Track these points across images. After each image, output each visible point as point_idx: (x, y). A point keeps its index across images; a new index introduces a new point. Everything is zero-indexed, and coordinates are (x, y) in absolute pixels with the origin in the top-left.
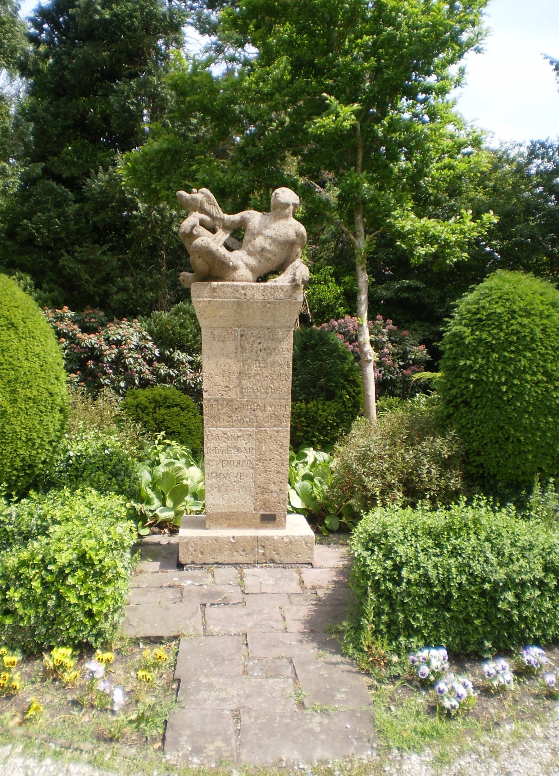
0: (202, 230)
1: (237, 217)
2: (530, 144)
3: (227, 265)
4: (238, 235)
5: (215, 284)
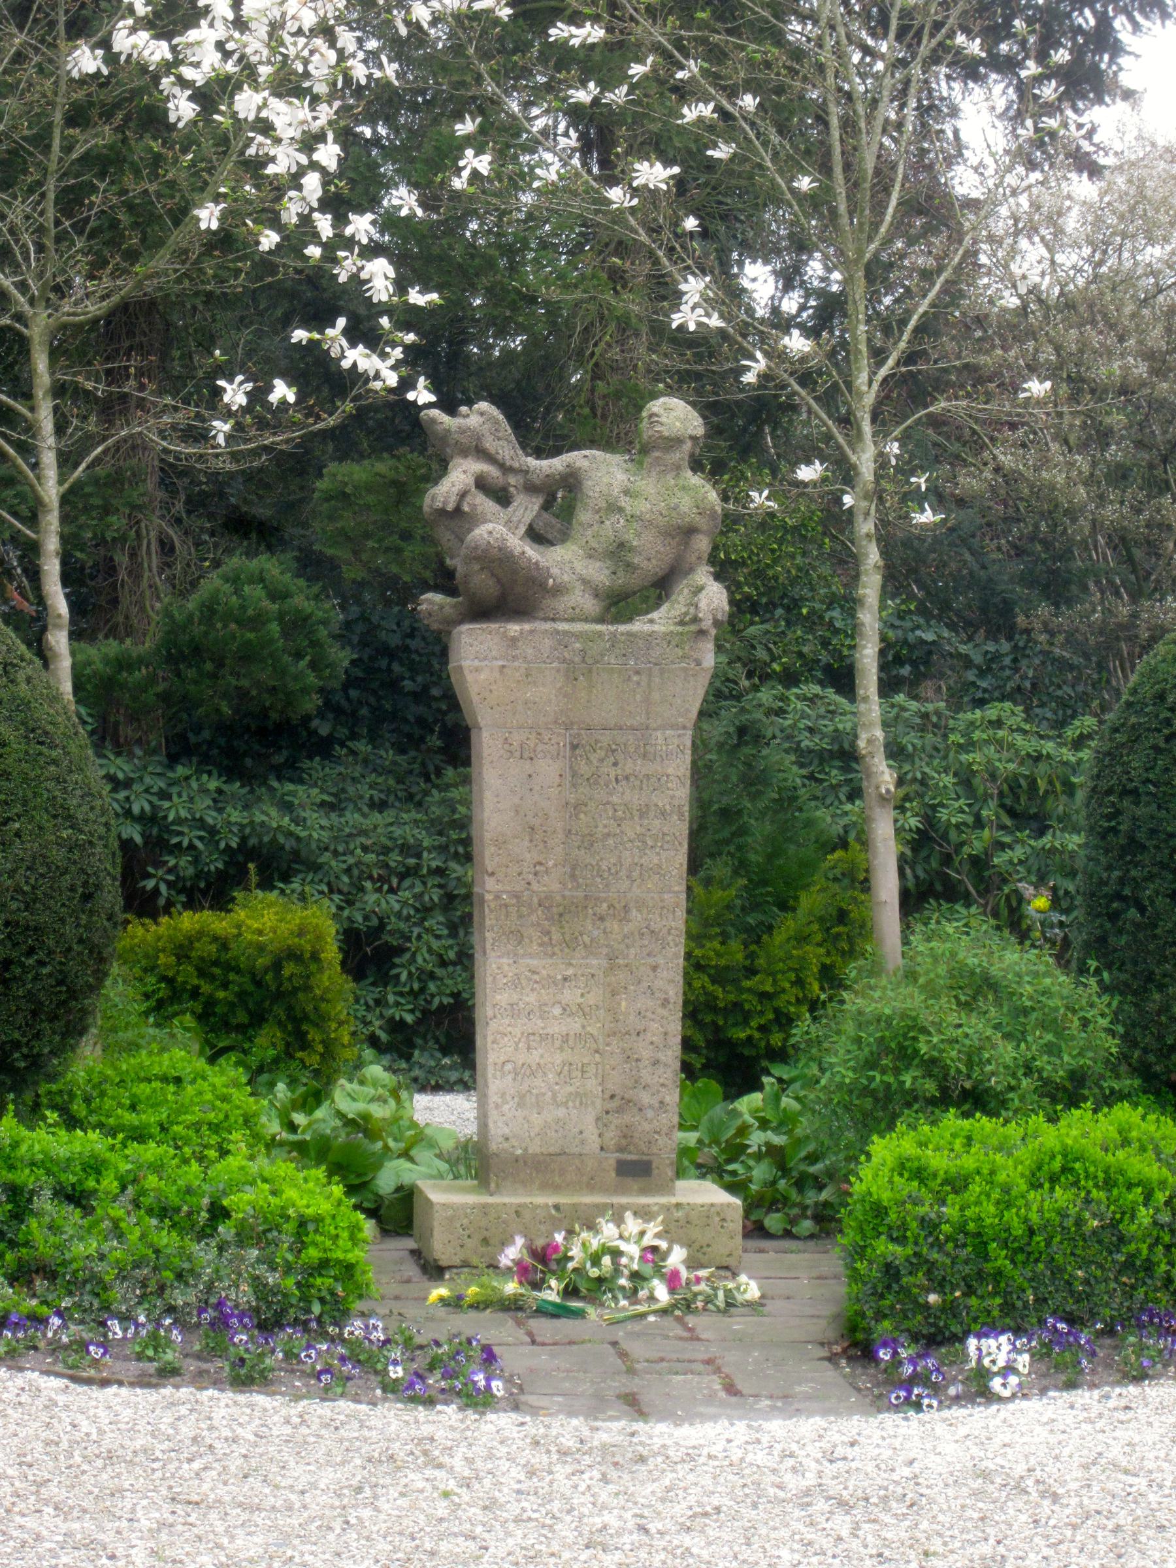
0: (485, 504)
1: (556, 464)
3: (543, 586)
4: (560, 502)
5: (514, 628)
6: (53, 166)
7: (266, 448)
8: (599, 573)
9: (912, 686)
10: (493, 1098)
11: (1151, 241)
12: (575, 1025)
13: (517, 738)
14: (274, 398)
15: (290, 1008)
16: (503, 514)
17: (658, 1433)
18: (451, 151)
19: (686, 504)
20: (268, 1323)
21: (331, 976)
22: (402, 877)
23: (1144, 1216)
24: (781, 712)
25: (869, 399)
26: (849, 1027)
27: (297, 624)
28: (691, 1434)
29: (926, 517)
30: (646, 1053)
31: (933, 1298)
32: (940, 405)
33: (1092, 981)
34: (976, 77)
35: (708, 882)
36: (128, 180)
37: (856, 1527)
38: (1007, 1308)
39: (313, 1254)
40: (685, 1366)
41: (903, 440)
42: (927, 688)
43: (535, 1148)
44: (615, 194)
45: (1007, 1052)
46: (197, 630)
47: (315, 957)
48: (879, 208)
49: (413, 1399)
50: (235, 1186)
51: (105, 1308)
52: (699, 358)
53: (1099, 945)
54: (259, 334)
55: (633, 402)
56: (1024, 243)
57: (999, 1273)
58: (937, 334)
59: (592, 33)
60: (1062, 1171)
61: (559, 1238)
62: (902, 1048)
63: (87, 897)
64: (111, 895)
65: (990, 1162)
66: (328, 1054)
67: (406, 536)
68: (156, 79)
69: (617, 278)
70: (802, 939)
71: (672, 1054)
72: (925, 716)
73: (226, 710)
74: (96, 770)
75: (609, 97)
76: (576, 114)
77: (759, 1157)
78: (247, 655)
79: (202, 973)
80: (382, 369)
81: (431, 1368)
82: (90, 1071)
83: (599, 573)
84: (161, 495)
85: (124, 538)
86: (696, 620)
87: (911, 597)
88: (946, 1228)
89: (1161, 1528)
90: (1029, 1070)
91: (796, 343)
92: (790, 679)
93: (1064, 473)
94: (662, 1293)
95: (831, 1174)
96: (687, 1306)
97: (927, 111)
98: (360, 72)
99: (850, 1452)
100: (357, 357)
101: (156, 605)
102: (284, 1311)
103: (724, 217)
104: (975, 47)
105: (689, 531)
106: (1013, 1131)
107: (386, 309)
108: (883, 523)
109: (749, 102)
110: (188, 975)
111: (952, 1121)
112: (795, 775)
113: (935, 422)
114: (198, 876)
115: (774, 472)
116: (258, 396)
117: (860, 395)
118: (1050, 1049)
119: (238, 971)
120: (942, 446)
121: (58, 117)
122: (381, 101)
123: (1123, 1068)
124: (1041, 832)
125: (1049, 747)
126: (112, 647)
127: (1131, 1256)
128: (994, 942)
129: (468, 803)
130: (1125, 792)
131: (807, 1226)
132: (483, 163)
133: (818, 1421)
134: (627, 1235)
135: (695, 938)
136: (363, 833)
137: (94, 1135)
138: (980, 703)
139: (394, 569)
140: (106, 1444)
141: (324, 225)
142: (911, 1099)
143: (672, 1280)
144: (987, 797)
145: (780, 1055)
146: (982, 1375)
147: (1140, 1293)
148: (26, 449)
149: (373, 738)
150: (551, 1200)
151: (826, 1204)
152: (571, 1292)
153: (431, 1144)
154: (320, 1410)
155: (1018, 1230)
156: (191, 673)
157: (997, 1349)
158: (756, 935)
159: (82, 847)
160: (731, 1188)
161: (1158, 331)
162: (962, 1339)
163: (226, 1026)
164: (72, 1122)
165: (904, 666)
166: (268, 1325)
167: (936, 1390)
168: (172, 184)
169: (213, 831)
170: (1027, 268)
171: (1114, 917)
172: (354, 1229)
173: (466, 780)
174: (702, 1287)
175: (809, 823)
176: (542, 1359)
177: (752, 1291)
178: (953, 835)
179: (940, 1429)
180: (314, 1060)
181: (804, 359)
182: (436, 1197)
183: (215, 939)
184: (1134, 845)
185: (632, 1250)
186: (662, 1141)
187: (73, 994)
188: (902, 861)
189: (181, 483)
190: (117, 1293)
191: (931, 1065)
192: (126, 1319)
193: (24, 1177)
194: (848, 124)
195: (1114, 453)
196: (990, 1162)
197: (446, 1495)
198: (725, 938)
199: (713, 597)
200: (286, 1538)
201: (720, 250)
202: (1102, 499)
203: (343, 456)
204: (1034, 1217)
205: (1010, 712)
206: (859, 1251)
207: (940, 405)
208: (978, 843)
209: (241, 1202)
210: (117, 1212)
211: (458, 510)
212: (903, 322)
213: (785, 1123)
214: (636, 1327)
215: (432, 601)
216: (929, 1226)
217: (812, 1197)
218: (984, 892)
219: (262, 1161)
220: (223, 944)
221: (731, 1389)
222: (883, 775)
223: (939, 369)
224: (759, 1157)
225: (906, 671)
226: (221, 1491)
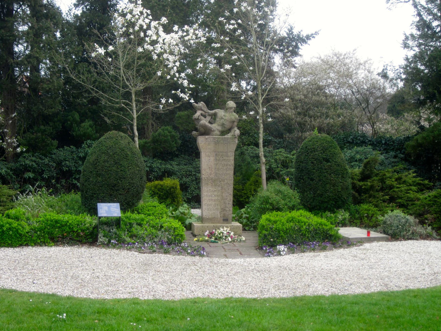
1: (213, 111)
2: (337, 52)
3: (211, 130)
5: (207, 137)
6: (135, 66)
7: (168, 109)
8: (220, 128)
9: (267, 146)
10: (204, 209)
11: (304, 78)
12: (216, 198)
13: (207, 154)
14: (169, 102)
15: (172, 196)
16: (205, 119)
17: (230, 260)
18: (196, 64)
19: (233, 117)
20: (169, 243)
21: (178, 190)
22: (189, 176)
23: (304, 227)
24: (247, 150)
25: (261, 102)
26: (258, 198)
27: (173, 137)
28: (235, 261)
29: (270, 120)
30: (227, 202)
31: (272, 240)
32: (272, 103)
33: (296, 191)
34: (277, 53)
35: (236, 176)
36: (147, 68)
37: (261, 275)
38: (283, 241)
39: (176, 233)
40: (233, 250)
41: (266, 108)
42: (270, 146)
43: (210, 217)
44: (222, 70)
45: (283, 202)
46: (157, 138)
47: (176, 188)
48: (263, 73)
49: (192, 255)
50: (164, 223)
51: (144, 241)
52: (235, 95)
53: (297, 185)
54: (166, 92)
55: (225, 103)
56: (284, 78)
57: (282, 236)
58: (271, 92)
59: (218, 45)
60: (292, 220)
61: (214, 231)
62: (267, 201)
63: (141, 178)
64: (145, 178)
65: (281, 219)
66: (178, 203)
67: (190, 123)
68: (151, 52)
69: (222, 83)
70: (251, 185)
71: (231, 202)
72: (269, 151)
73: (162, 150)
74: (143, 159)
75: (221, 55)
76: (215, 58)
77: (244, 218)
78: (165, 142)
79: (158, 190)
80: (186, 97)
81: (195, 251)
82: (141, 205)
83: (220, 128)
84: (152, 117)
85: (146, 124)
86: (235, 135)
87: (267, 132)
88: (274, 229)
89: (308, 275)
90: (286, 205)
91: (250, 93)
92: (249, 145)
93: (291, 113)
94: (230, 239)
95: (256, 221)
96: (234, 241)
97: (269, 58)
98: (183, 51)
99: (259, 263)
100: (182, 95)
101: (151, 134)
102: (172, 242)
103: (238, 74)
104: (277, 47)
105: (234, 122)
106: (284, 214)
107: (186, 88)
108: (263, 121)
109: (242, 56)
110: (156, 191)
111: (274, 212)
112: (249, 160)
113: (271, 105)
114: (158, 176)
115: (246, 113)
116: (167, 101)
117: (260, 101)
118: (290, 202)
119: (164, 190)
120: (273, 109)
121: (136, 58)
122: (184, 56)
123: (301, 205)
124: (287, 169)
125: (289, 155)
126: (144, 140)
127: (302, 233)
128: (281, 185)
129: (200, 164)
130: (301, 162)
131: (252, 229)
132: (201, 65)
133: (254, 259)
134: (224, 230)
135: (234, 185)
136: (183, 169)
137: (142, 215)
138: (278, 149)
139: (188, 128)
140: (145, 262)
141: (177, 75)
142: (268, 209)
143: (231, 237)
144: (279, 163)
145: (248, 203)
146: (279, 251)
147: (304, 239)
148: (131, 110)
149: (184, 154)
150: (213, 225)
151: (255, 226)
152: (216, 239)
153: (194, 217)
154: (178, 257)
155: (285, 229)
156: (156, 144)
157: (282, 248)
158: (244, 184)
159: (140, 171)
160: (240, 223)
161: (305, 91)
162: (276, 246)
163: (162, 198)
164: (139, 213)
165: (266, 143)
166: (169, 244)
167: (272, 254)
168: (153, 69)
169: (160, 169)
170: (286, 81)
171: (299, 181)
172: (182, 229)
173: (200, 161)
174: (236, 238)
175: (252, 167)
176: (212, 249)
177: (244, 239)
178: (274, 169)
179: (273, 260)
180: (176, 204)
181: (251, 95)
182: (195, 224)
183: (161, 185)
184: (302, 170)
185: (225, 232)
186: (230, 216)
187: (139, 193)
188: (266, 173)
189: (155, 115)
190: (146, 239)
191: (271, 204)
192: (147, 243)
193: (132, 221)
194: (258, 60)
195: (299, 110)
196: (281, 219)
197: (197, 270)
198: (239, 185)
199: (237, 132)
200: (173, 277)
201: (239, 77)
202: (297, 117)
203: (180, 111)
204: (287, 227)
205: (283, 150)
206: (260, 233)
207: (272, 103)
208: (278, 170)
209: (165, 225)
210: (146, 227)
211: (198, 118)
212: (266, 90)
213: (248, 213)
214: (226, 244)
215: (194, 133)
216: (271, 229)
217: (253, 225)
218: (279, 178)
219: (168, 219)
220: (162, 186)
221: (241, 254)
222: (263, 160)
223: (272, 98)
224: (244, 218)
225: (266, 144)
226: (163, 269)
